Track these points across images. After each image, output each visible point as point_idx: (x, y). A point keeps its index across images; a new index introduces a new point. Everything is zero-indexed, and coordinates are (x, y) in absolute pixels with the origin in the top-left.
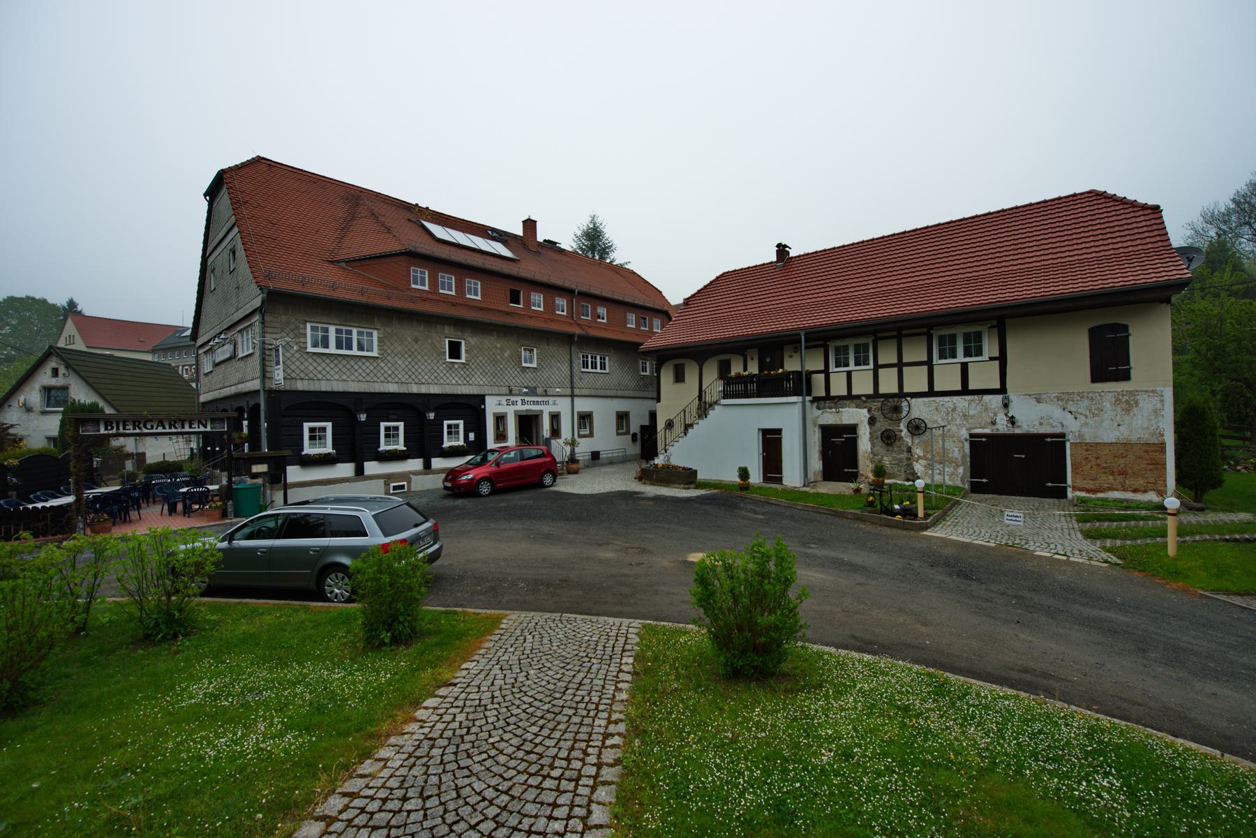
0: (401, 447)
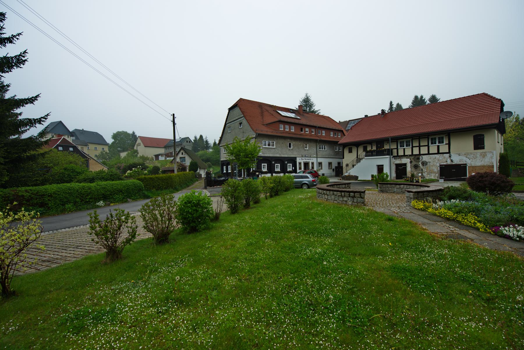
0: (279, 170)
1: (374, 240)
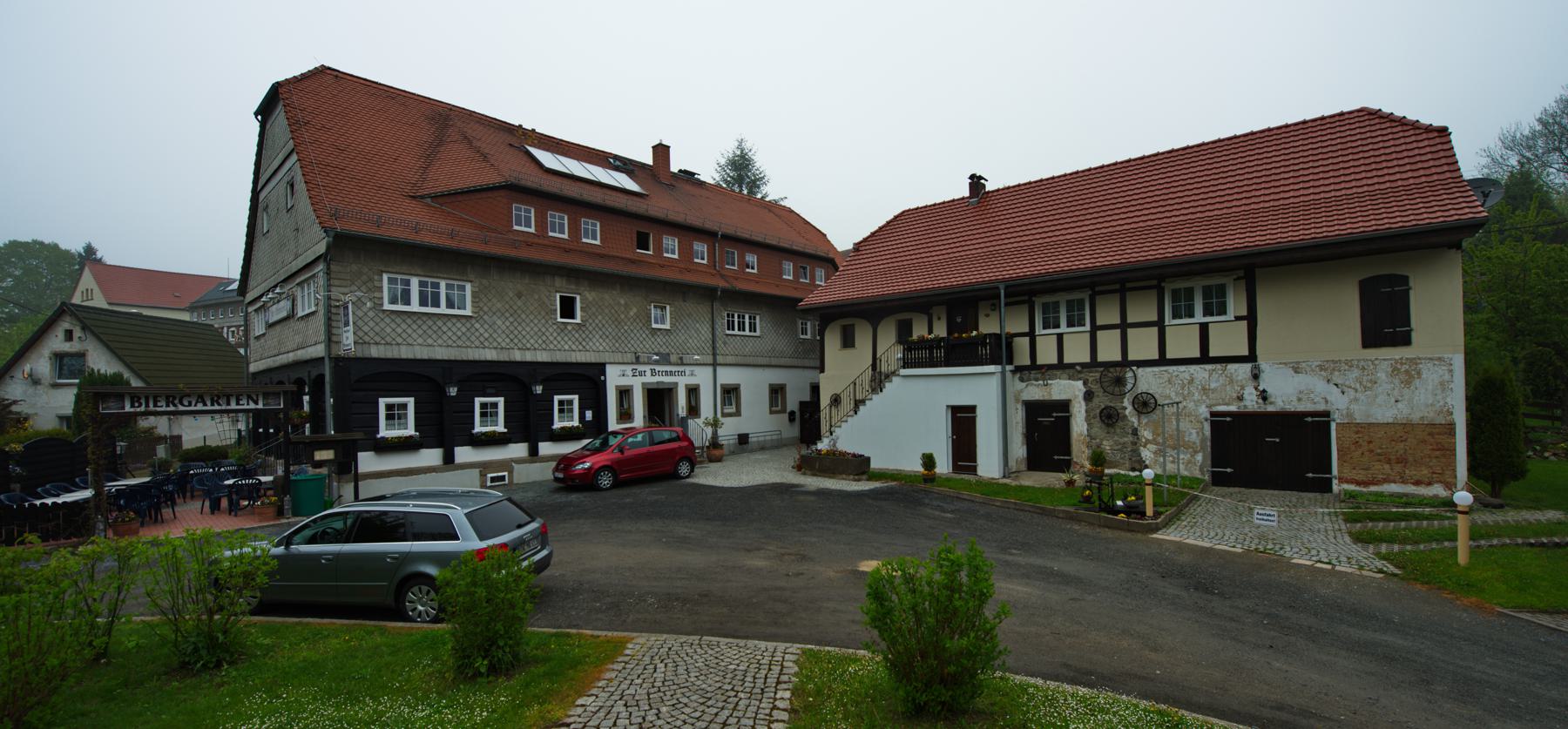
0: (500, 428)
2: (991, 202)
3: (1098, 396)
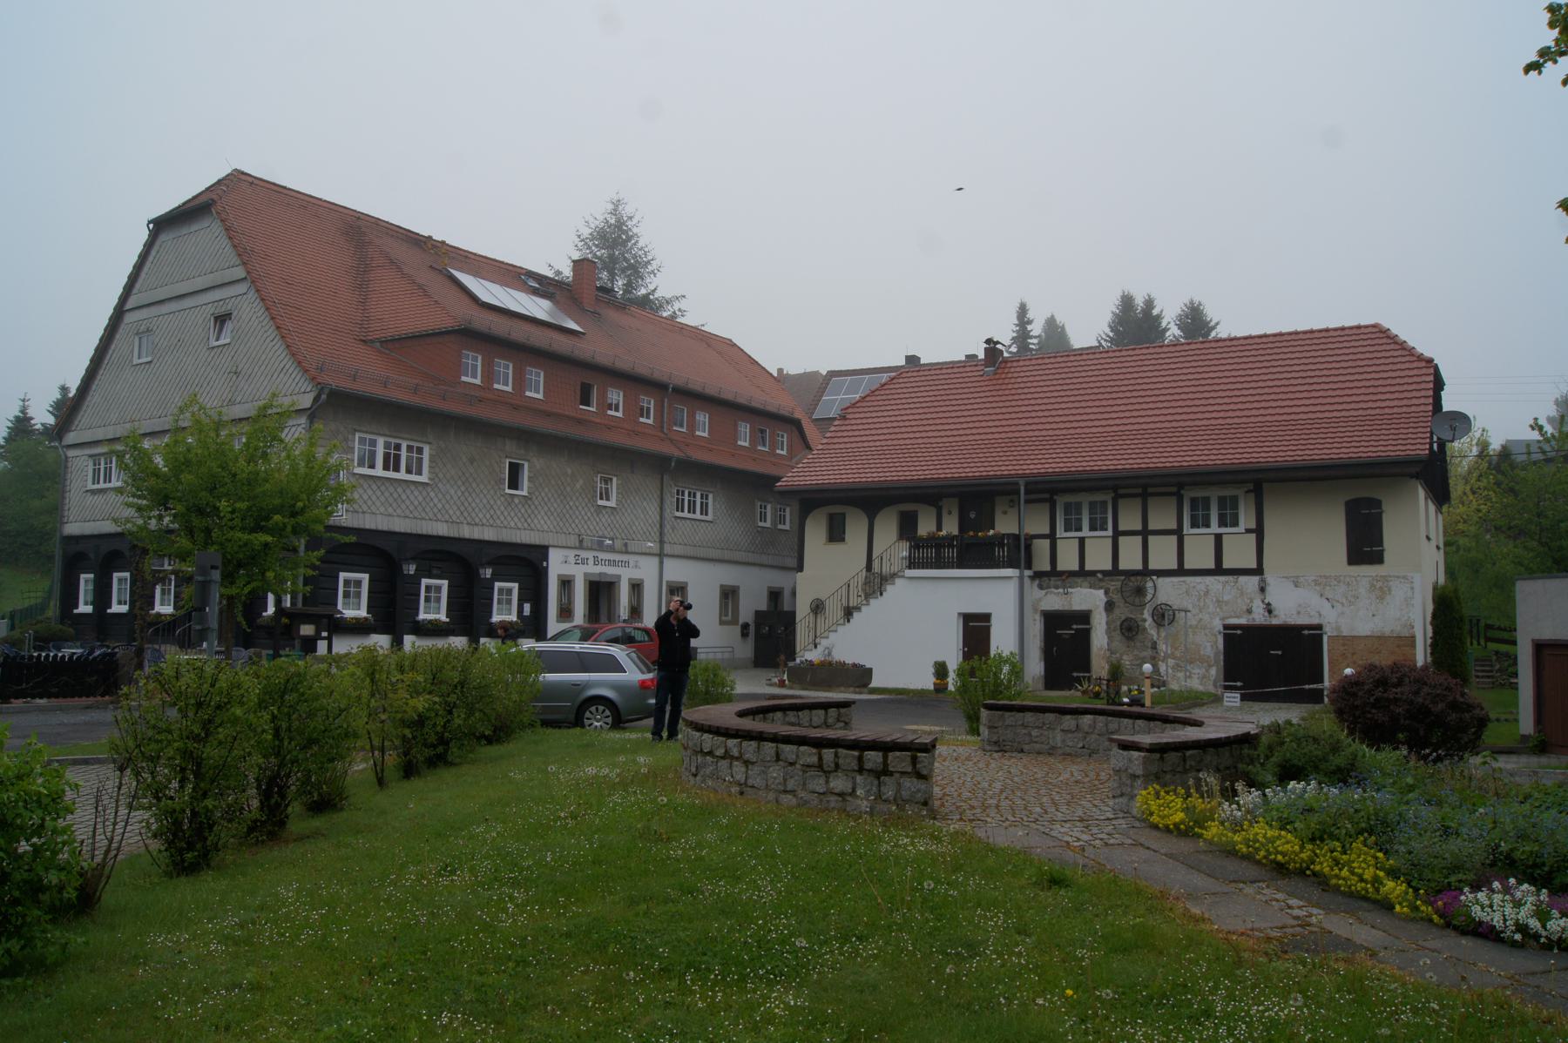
0: (443, 617)
1: (998, 983)
2: (1010, 375)
3: (1119, 607)
